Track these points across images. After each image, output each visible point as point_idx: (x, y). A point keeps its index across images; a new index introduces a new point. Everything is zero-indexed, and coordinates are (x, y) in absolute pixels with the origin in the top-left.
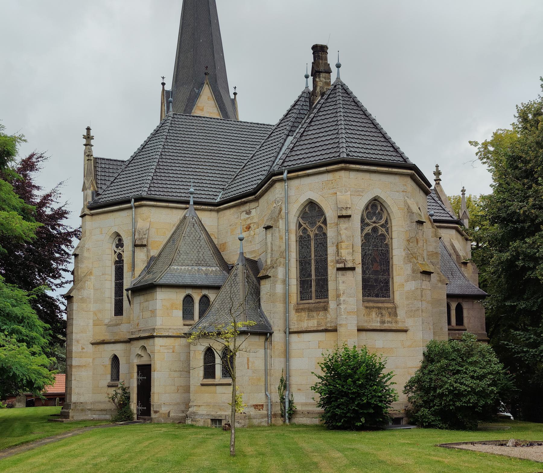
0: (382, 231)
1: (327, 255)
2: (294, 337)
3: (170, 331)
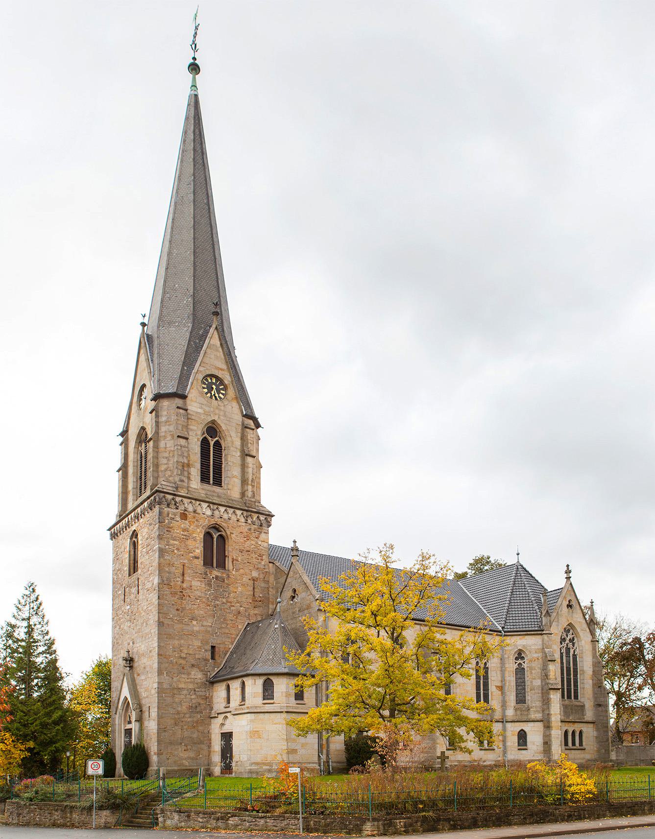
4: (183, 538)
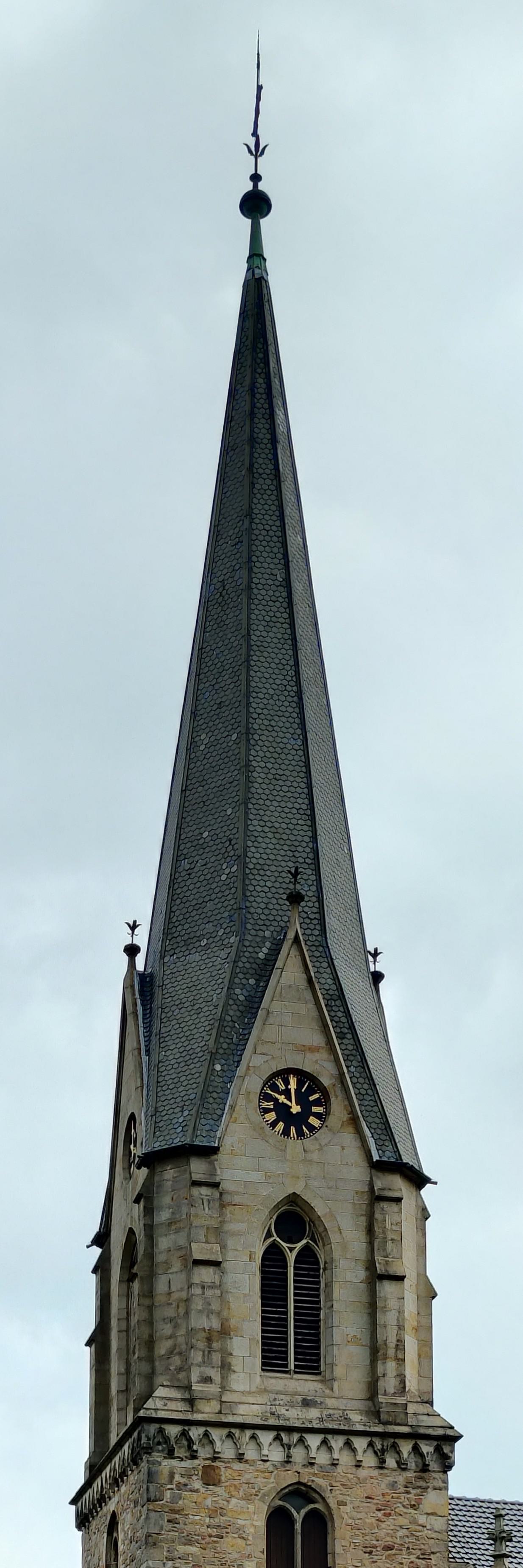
4: (210, 1536)
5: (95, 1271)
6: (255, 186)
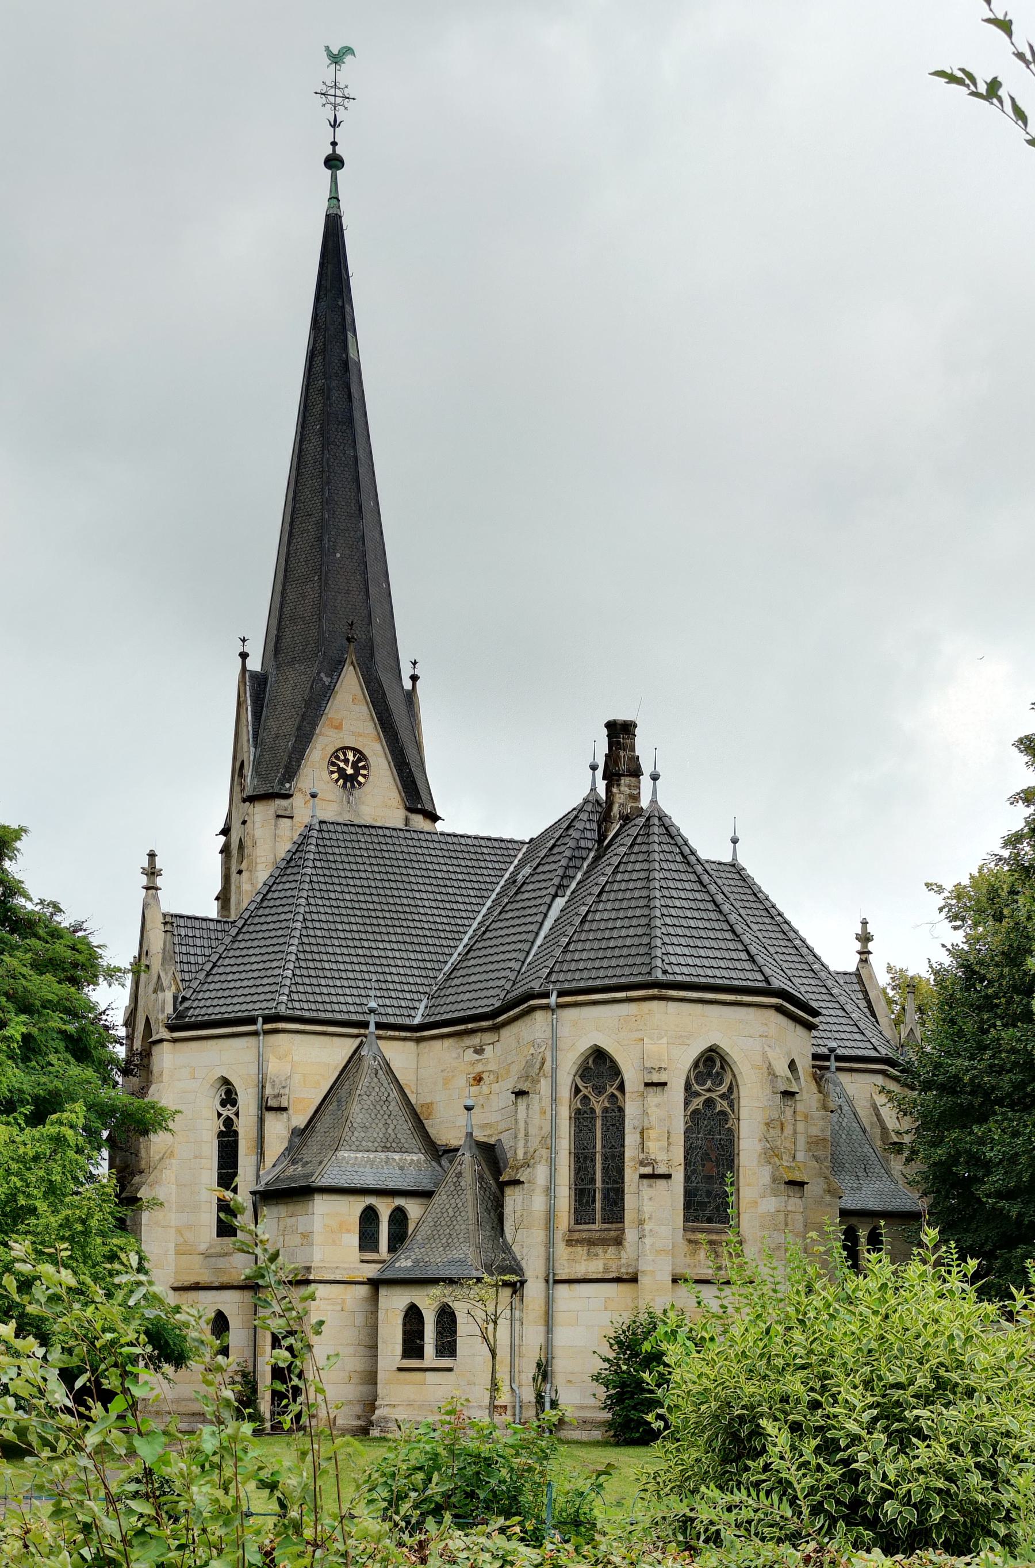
0: (722, 1105)
1: (623, 1146)
2: (562, 1290)
3: (338, 1271)
5: (221, 852)
6: (334, 150)
